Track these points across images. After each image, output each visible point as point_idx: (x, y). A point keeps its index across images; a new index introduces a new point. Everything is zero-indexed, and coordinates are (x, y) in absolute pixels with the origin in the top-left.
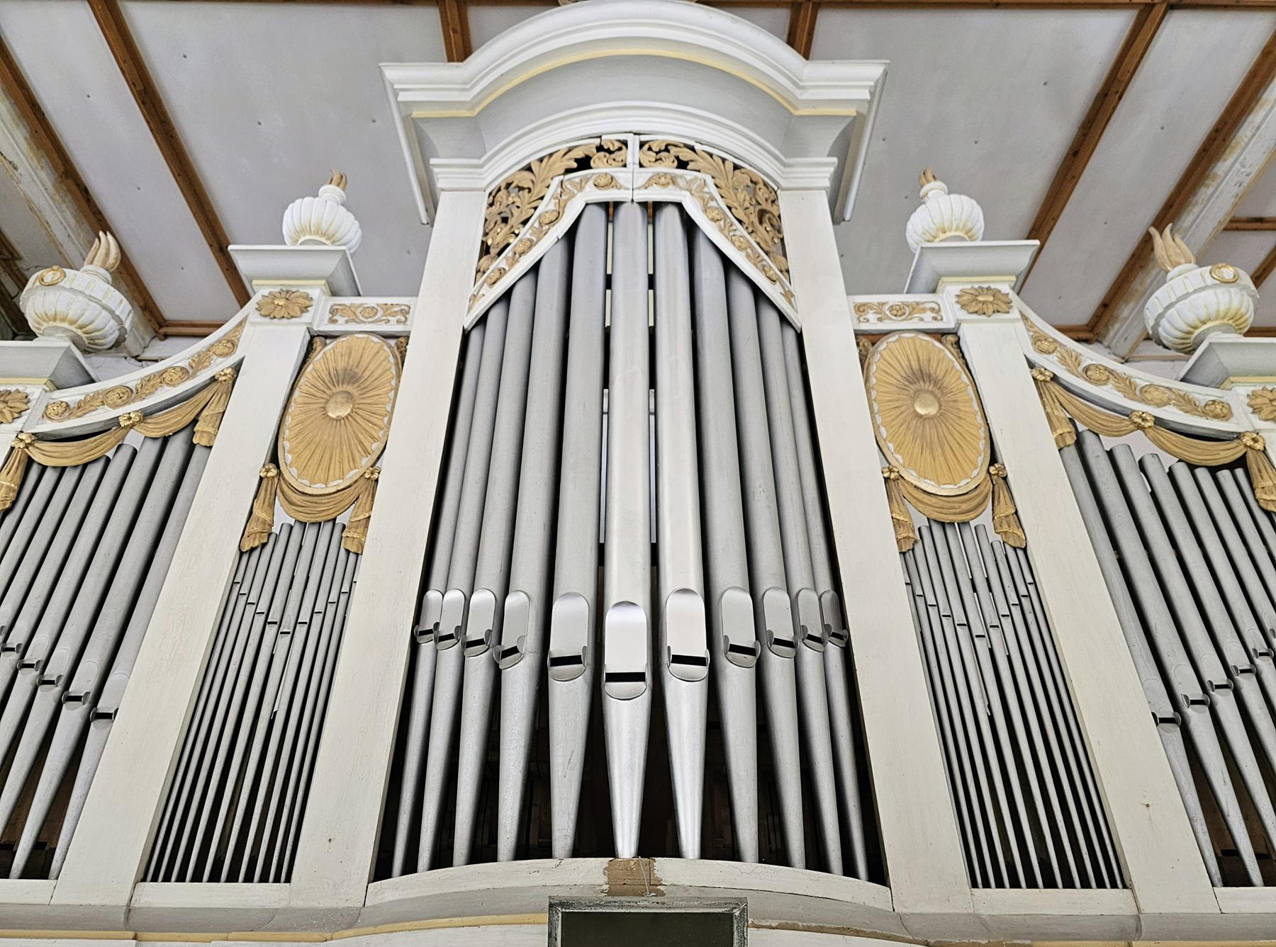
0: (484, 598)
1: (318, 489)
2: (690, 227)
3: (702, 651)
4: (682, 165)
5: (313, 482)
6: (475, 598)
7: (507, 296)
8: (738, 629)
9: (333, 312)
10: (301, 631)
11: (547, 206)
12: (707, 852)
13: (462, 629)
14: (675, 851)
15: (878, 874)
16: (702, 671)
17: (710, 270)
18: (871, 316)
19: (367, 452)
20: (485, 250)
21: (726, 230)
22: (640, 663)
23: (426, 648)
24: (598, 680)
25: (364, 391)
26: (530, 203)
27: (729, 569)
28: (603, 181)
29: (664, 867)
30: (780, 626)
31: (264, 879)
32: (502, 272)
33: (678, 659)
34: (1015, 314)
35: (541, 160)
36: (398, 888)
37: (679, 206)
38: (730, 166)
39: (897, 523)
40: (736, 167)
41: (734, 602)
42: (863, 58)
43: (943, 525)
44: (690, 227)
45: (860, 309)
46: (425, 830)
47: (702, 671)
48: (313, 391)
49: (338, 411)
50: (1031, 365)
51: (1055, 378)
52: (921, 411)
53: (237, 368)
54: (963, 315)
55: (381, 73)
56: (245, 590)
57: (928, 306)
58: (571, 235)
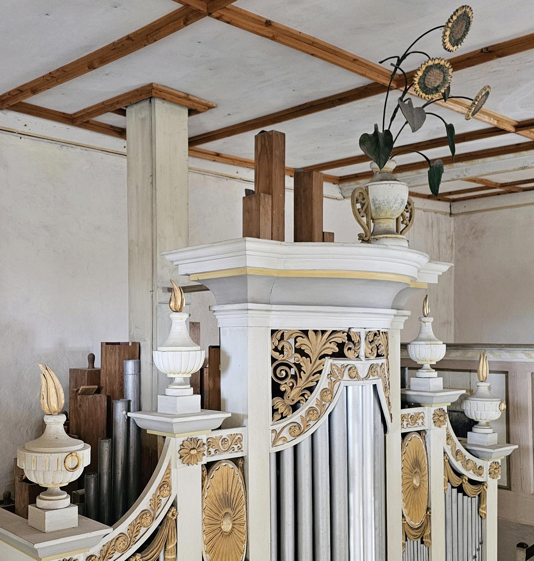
11: (324, 382)
20: (277, 392)
26: (313, 375)
35: (316, 332)
48: (212, 514)
52: (415, 482)
57: (421, 415)
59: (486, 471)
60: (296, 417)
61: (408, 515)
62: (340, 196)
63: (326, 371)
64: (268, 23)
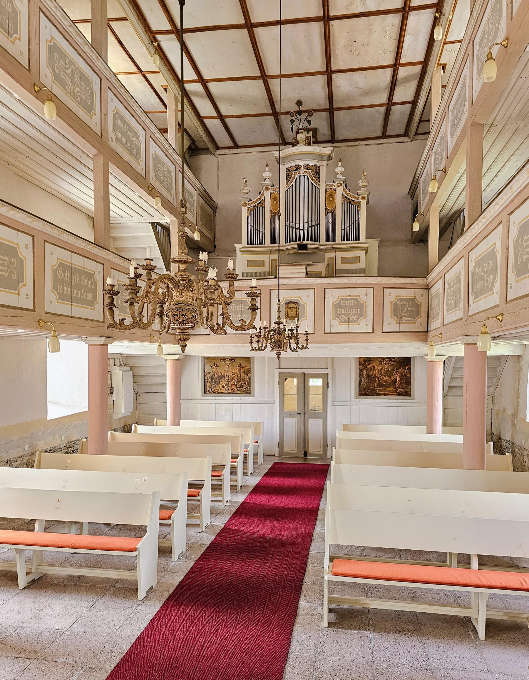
0: (291, 223)
1: (331, 209)
2: (308, 179)
7: (290, 188)
8: (314, 224)
9: (272, 189)
11: (293, 176)
12: (311, 241)
14: (305, 241)
15: (319, 242)
17: (314, 187)
18: (328, 187)
20: (287, 180)
21: (313, 179)
22: (302, 228)
23: (287, 227)
24: (300, 230)
29: (304, 242)
32: (289, 185)
34: (342, 186)
36: (287, 244)
40: (314, 166)
42: (427, 249)
49: (275, 203)
50: (342, 193)
56: (251, 224)
58: (296, 180)
59: (360, 198)
60: (288, 183)
62: (409, 140)
63: (294, 173)
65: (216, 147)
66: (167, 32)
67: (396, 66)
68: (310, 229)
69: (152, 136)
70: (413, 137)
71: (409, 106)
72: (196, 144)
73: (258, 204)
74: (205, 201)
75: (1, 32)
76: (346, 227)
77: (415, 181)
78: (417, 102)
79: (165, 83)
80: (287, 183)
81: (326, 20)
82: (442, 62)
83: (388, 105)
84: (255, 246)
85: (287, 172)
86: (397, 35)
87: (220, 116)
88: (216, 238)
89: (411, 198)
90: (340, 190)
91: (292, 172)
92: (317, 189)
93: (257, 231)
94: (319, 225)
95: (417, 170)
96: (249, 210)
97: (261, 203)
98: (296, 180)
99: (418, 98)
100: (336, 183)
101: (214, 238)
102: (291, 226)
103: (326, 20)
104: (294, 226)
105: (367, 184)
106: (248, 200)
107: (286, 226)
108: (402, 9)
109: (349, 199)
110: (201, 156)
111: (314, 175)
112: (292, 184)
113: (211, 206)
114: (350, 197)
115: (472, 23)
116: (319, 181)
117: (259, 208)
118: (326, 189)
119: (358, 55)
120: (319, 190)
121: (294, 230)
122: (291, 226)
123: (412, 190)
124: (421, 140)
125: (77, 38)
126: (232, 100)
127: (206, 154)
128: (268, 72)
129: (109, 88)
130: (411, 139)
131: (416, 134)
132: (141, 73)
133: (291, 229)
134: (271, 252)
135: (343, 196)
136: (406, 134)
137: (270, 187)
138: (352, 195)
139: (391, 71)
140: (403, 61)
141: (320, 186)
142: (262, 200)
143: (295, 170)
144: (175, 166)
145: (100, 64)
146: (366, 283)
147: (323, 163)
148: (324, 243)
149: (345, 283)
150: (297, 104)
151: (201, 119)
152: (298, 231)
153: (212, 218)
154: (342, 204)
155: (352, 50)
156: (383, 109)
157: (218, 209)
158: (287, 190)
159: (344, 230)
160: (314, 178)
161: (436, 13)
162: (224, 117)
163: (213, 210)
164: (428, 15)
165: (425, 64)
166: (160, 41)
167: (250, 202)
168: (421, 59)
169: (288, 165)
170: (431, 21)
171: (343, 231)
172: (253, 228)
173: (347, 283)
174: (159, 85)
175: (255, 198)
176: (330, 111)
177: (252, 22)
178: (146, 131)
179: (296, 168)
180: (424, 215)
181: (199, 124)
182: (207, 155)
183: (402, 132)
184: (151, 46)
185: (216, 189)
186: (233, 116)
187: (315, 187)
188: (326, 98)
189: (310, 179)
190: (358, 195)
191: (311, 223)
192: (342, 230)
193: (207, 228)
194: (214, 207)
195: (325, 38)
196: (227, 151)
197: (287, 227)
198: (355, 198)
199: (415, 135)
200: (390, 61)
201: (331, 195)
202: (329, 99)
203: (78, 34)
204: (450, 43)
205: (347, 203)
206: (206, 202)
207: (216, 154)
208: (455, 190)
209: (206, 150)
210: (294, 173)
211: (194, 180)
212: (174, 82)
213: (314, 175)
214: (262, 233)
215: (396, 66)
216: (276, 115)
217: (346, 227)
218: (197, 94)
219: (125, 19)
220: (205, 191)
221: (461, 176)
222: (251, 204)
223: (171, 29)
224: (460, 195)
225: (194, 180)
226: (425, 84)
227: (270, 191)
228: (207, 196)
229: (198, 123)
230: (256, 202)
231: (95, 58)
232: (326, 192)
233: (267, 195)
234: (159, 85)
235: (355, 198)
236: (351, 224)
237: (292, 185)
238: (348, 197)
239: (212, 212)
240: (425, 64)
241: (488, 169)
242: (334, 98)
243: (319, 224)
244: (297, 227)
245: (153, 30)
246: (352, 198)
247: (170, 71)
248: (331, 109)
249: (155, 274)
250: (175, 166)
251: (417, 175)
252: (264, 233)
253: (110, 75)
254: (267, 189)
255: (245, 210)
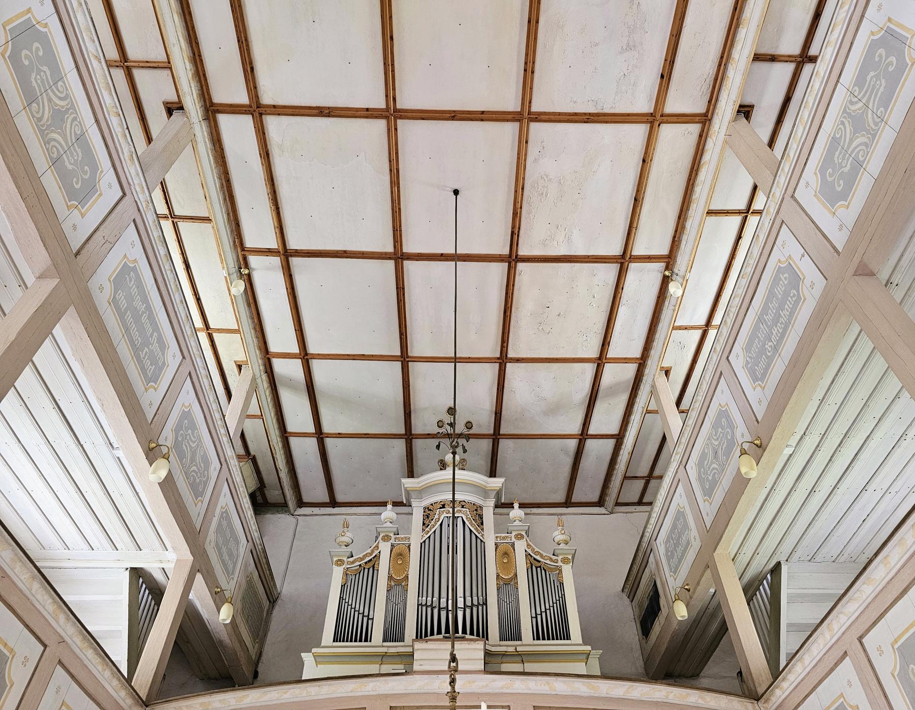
0: (429, 599)
2: (464, 523)
3: (463, 607)
4: (463, 507)
5: (397, 577)
6: (428, 599)
7: (429, 537)
8: (469, 603)
9: (395, 539)
10: (558, 602)
11: (436, 516)
13: (426, 604)
16: (463, 609)
17: (474, 537)
18: (499, 539)
19: (406, 571)
20: (424, 524)
21: (472, 524)
23: (420, 607)
25: (404, 557)
27: (468, 593)
28: (447, 512)
30: (475, 603)
31: (400, 642)
32: (428, 532)
33: (459, 608)
34: (525, 540)
35: (435, 503)
37: (462, 517)
38: (472, 504)
39: (497, 584)
40: (474, 504)
41: (468, 599)
43: (505, 584)
44: (464, 523)
45: (497, 537)
46: (798, 174)
47: (463, 609)
50: (526, 551)
51: (529, 554)
53: (380, 552)
54: (515, 540)
55: (401, 481)
58: (441, 525)
59: (559, 561)
60: (427, 529)
61: (502, 575)
63: (437, 513)
64: (428, 434)
65: (298, 500)
66: (268, 252)
67: (601, 361)
68: (468, 611)
69: (193, 374)
70: (613, 509)
71: (611, 443)
72: (266, 492)
73: (366, 563)
74: (259, 574)
75: (1, 248)
76: (539, 612)
77: (640, 554)
78: (624, 436)
79: (241, 357)
80: (423, 530)
81: (513, 260)
82: (666, 364)
83: (581, 437)
84: (349, 644)
85: (424, 512)
86: (608, 304)
87: (320, 435)
88: (264, 658)
89: (628, 597)
90: (521, 547)
91: (434, 511)
92: (479, 541)
93: (359, 614)
94: (485, 607)
95: (645, 527)
96: (346, 575)
97: (372, 564)
98: (441, 525)
99: (625, 430)
100: (514, 534)
101: (258, 656)
102: (429, 604)
103: (513, 260)
104: (436, 604)
105: (569, 538)
106: (348, 554)
107: (418, 605)
108: (621, 257)
109: (539, 561)
110: (269, 516)
111: (474, 518)
112: (433, 530)
113: (268, 590)
114: (542, 558)
115: (786, 170)
116: (482, 529)
117: (366, 570)
118: (496, 544)
119: (549, 333)
120: (483, 543)
121: (436, 611)
122: (429, 604)
123: (632, 578)
124: (624, 513)
125: (103, 91)
126: (345, 402)
127: (279, 514)
128: (411, 352)
129: (134, 220)
130: (610, 509)
131: (617, 504)
132: (208, 330)
133: (429, 609)
134: (384, 660)
135: (528, 555)
136: (600, 503)
137: (392, 535)
138: (544, 555)
139: (594, 367)
140: (611, 354)
141: (485, 537)
142: (374, 558)
143: (441, 508)
144: (222, 465)
145: (133, 172)
146: (633, 700)
147: (488, 502)
148: (498, 642)
149: (582, 694)
150: (448, 412)
151: (285, 435)
152: (443, 614)
153: (265, 615)
154: (527, 570)
155: (541, 323)
156: (573, 444)
157: (279, 602)
158: (424, 541)
159: (536, 617)
160: (474, 522)
161: (665, 271)
162: (325, 435)
163: (270, 602)
164: (655, 271)
165: (642, 362)
166: (254, 269)
167: (351, 559)
168: (637, 354)
169: (427, 502)
170: (657, 287)
171: (534, 620)
172: (349, 607)
173: (586, 695)
174: (231, 360)
175: (361, 553)
176: (494, 437)
177: (404, 250)
178: (184, 358)
179: (442, 505)
180: (688, 590)
181: (280, 446)
182: (281, 515)
183: (595, 497)
184: (235, 274)
185: (284, 567)
186: (340, 436)
187: (477, 537)
188: (491, 411)
189: (467, 522)
190: (554, 555)
191: (470, 598)
192: (532, 617)
193: (249, 627)
194: (273, 598)
195: (507, 293)
196: (316, 510)
197: (420, 607)
198: (551, 560)
199: (615, 506)
200: (594, 353)
201: (505, 555)
202: (496, 414)
203: (108, 83)
204: (680, 328)
205: (537, 568)
206: (260, 577)
207: (295, 513)
208: (768, 504)
209: (282, 507)
210: (437, 513)
211: (249, 517)
212: (258, 352)
213: (474, 518)
214: (368, 619)
215: (601, 361)
216: (411, 437)
217: (539, 612)
218: (291, 384)
219: (207, 220)
220: (263, 552)
221: (791, 455)
222: (353, 562)
223: (277, 247)
224: (771, 524)
225: (249, 517)
226: (638, 401)
227: (392, 541)
228: (266, 566)
229: (279, 443)
230: (362, 559)
231: (126, 154)
232: (496, 549)
233: (385, 548)
234: (231, 360)
235: (551, 560)
236: (555, 601)
237: (435, 531)
238: (538, 558)
239: (266, 603)
240: (642, 362)
241: (841, 442)
242: (503, 413)
243: (486, 605)
244: (441, 606)
245: (247, 246)
246: (544, 559)
247: (256, 331)
248: (496, 436)
249: (81, 633)
250: (222, 465)
251: (647, 535)
252: (373, 619)
253: (147, 206)
254: (386, 538)
255: (338, 575)
